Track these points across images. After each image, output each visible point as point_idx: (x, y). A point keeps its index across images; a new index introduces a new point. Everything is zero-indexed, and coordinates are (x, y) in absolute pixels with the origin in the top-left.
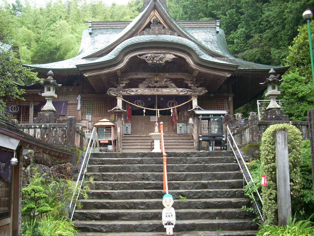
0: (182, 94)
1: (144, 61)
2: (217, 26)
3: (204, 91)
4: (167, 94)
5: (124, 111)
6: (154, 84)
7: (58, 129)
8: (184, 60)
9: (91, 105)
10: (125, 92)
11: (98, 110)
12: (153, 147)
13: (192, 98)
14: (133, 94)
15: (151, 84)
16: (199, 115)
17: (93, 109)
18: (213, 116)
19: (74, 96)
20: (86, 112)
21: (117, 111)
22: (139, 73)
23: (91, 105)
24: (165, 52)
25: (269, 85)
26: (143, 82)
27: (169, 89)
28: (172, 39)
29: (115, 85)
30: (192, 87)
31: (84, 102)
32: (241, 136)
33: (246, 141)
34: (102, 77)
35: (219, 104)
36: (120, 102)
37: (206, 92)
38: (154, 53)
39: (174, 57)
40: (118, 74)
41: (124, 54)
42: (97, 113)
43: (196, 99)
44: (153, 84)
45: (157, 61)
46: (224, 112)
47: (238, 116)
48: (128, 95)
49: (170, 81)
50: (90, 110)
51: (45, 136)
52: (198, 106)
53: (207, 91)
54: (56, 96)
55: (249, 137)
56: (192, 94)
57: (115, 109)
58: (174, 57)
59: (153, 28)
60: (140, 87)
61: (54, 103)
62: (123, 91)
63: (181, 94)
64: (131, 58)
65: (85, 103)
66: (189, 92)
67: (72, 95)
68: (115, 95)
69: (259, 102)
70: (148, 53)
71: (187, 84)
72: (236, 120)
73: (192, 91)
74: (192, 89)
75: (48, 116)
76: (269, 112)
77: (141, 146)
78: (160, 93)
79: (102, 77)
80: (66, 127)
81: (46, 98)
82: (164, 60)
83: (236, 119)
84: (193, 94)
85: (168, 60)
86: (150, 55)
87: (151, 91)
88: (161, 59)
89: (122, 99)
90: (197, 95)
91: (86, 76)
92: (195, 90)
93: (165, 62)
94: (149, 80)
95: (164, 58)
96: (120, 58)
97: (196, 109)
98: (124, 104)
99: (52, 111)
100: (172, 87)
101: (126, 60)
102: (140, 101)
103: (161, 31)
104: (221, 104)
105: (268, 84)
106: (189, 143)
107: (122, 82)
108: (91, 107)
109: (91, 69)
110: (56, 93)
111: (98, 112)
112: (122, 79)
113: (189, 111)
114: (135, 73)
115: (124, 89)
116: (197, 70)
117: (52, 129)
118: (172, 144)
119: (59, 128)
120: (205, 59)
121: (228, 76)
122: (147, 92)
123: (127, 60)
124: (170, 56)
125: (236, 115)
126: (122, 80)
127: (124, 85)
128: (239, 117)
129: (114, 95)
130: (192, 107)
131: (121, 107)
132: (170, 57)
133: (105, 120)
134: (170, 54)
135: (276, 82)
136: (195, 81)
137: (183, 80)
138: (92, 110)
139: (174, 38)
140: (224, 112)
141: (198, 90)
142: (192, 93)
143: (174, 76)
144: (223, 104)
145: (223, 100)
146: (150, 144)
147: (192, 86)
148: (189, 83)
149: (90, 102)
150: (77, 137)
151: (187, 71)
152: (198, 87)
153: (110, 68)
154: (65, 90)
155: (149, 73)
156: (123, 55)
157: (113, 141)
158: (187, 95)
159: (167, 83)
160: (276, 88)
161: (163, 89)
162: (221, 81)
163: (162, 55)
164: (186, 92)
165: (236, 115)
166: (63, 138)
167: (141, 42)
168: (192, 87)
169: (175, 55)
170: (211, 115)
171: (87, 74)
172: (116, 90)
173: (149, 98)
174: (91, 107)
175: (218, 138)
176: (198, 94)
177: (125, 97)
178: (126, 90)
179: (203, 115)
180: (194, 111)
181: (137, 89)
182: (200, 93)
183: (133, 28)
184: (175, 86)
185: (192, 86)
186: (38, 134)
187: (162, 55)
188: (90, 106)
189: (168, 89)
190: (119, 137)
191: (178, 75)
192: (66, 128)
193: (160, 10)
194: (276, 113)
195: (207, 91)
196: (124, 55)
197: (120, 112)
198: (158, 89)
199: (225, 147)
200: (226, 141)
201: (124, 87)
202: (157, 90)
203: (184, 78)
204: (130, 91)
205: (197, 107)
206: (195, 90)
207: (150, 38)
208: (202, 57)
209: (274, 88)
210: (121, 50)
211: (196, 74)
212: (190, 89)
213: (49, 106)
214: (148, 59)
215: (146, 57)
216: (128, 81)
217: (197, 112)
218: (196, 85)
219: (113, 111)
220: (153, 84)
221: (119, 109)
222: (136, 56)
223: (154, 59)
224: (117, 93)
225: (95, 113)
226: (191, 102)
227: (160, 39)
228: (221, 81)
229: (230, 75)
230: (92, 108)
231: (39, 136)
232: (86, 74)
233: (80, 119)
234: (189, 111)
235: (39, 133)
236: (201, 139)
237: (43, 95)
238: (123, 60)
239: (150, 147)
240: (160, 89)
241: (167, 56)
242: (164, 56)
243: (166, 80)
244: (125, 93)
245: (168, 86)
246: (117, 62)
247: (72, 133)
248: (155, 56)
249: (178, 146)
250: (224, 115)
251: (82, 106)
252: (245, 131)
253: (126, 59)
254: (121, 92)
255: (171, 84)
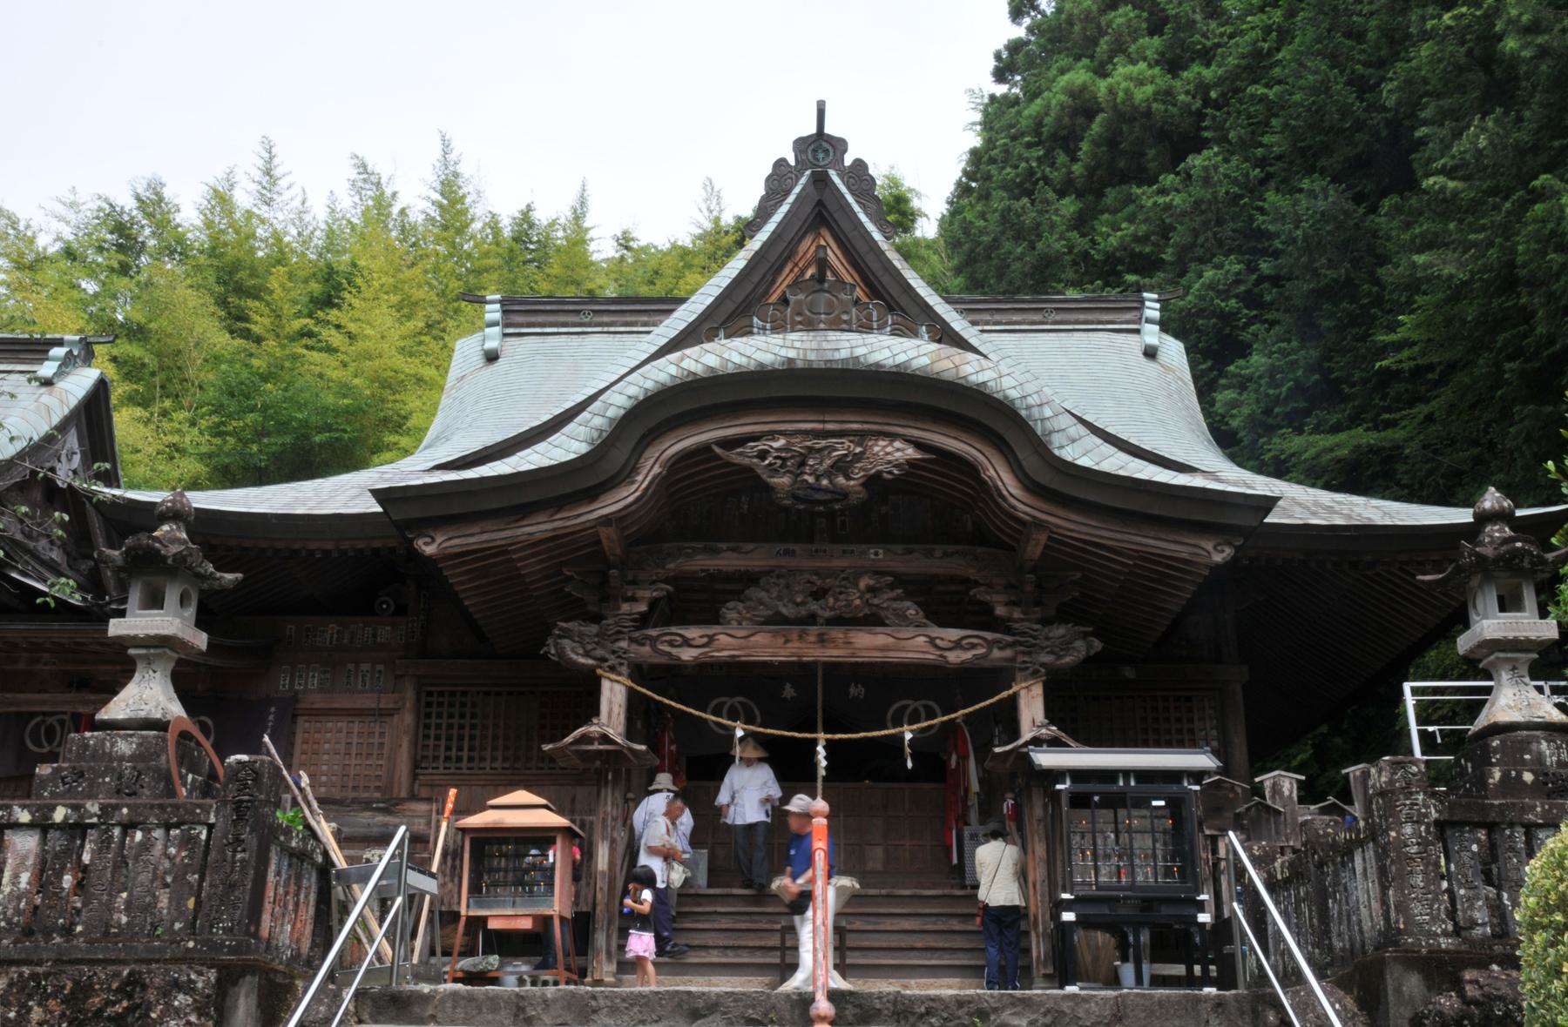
0: (958, 661)
1: (750, 481)
2: (1149, 321)
3: (1079, 644)
4: (877, 656)
5: (630, 749)
6: (803, 603)
7: (158, 833)
8: (969, 469)
9: (467, 721)
10: (643, 645)
11: (506, 748)
12: (788, 960)
13: (1014, 680)
14: (687, 655)
15: (790, 605)
16: (1056, 775)
17: (477, 743)
18: (1137, 781)
19: (380, 667)
20: (436, 758)
21: (596, 746)
22: (724, 546)
23: (467, 721)
24: (866, 427)
25: (1480, 586)
26: (747, 592)
27: (888, 630)
28: (901, 358)
29: (592, 608)
30: (1016, 621)
31: (429, 704)
32: (1321, 898)
33: (1361, 932)
34: (520, 560)
35: (1167, 720)
36: (613, 696)
37: (1092, 652)
38: (805, 433)
39: (911, 452)
40: (605, 542)
41: (638, 436)
42: (497, 764)
43: (1038, 690)
44: (798, 605)
45: (818, 478)
46: (1202, 760)
47: (1276, 789)
48: (663, 660)
49: (892, 587)
50: (460, 749)
51: (68, 881)
52: (1052, 722)
53: (1098, 645)
54: (201, 640)
55: (1375, 905)
56: (1013, 659)
57: (585, 739)
58: (911, 452)
59: (799, 302)
60: (729, 623)
61: (183, 688)
62: (632, 640)
63: (954, 657)
64: (673, 464)
65: (434, 710)
66: (1001, 649)
67: (365, 667)
68: (591, 662)
69: (1415, 691)
70: (772, 435)
71: (987, 609)
72: (1268, 808)
73: (1012, 645)
74: (1014, 635)
75: (132, 758)
76: (1496, 750)
77: (729, 952)
78: (835, 652)
79: (520, 560)
80: (212, 820)
81: (132, 651)
82: (858, 475)
83: (1269, 802)
84: (1020, 658)
85: (879, 474)
86: (781, 442)
87: (787, 642)
88: (842, 466)
89: (629, 683)
90: (1042, 665)
91: (429, 550)
92: (1035, 638)
93: (863, 485)
94: (777, 585)
95: (858, 457)
96: (620, 455)
97: (1036, 742)
98: (635, 705)
99: (160, 725)
100: (904, 620)
101: (650, 469)
102: (741, 699)
103: (845, 317)
104: (1179, 720)
105: (1474, 582)
106: (738, 921)
107: (629, 594)
108: (467, 732)
109: (455, 511)
110: (201, 623)
111: (505, 759)
112: (630, 577)
113: (997, 750)
114: (700, 545)
115: (637, 629)
116: (1039, 525)
117: (117, 832)
118: (907, 941)
119: (168, 827)
120: (1084, 462)
121: (1218, 558)
122: (766, 647)
123: (657, 469)
124: (889, 449)
125: (1267, 779)
126: (634, 582)
127: (643, 608)
128: (1281, 793)
129: (582, 660)
130: (1014, 733)
131: (621, 728)
132: (892, 453)
133: (522, 796)
134: (893, 437)
135: (1526, 564)
136: (1029, 588)
137: (967, 582)
138: (471, 749)
139: (911, 354)
140: (1202, 760)
141: (1047, 638)
142: (1017, 653)
143: (916, 564)
144: (1191, 720)
145: (1189, 699)
146: (774, 941)
147: (1017, 614)
148: (997, 598)
149: (463, 705)
150: (293, 888)
151: (980, 537)
152: (1046, 622)
153: (560, 509)
154: (328, 636)
155: (780, 547)
156: (633, 443)
157: (562, 919)
158: (987, 664)
159: (876, 601)
160: (1530, 599)
161: (852, 634)
162: (1176, 587)
163: (843, 447)
164: (981, 651)
165: (1267, 784)
166: (179, 890)
167: (730, 369)
168: (1016, 621)
169: (918, 445)
170: (1127, 773)
171: (433, 540)
172: (597, 635)
173: (788, 686)
174: (467, 732)
175: (1165, 910)
176: (1046, 658)
177: (640, 673)
178: (653, 632)
179: (1079, 775)
180: (1027, 754)
181: (711, 630)
182: (1060, 657)
183: (705, 320)
184: (921, 613)
185: (1017, 614)
186: (21, 865)
187: (843, 447)
188: (461, 727)
189: (879, 629)
190: (599, 896)
191: (938, 554)
192: (211, 827)
193: (845, 225)
194: (1539, 758)
195: (1098, 645)
196: (638, 443)
197: (608, 752)
198: (824, 629)
199: (1213, 968)
200: (1224, 926)
201: (643, 621)
202: (822, 640)
203: (971, 573)
204: (671, 644)
205: (1044, 731)
206: (1035, 638)
207: (783, 352)
208: (1068, 454)
209: (1508, 603)
210: (622, 412)
211: (1035, 548)
212: (1008, 631)
213: (147, 694)
214: (770, 464)
215: (763, 455)
216: (663, 586)
217: (1046, 759)
218: (1038, 612)
219: (574, 748)
220: (798, 605)
221: (605, 739)
222: (705, 449)
223: (803, 464)
224: (599, 652)
225: (487, 764)
226: (1013, 702)
227: (837, 356)
228: (1176, 587)
229: (1228, 552)
230: (472, 738)
231: (25, 877)
232: (426, 544)
233: (404, 794)
234: (997, 750)
235: (24, 858)
236: (1068, 916)
237: (116, 628)
238: (634, 470)
239: (777, 961)
240: (837, 633)
241: (876, 449)
242: (858, 450)
243: (872, 582)
244: (647, 649)
245: (882, 614)
246: (602, 478)
247: (242, 860)
248: (810, 449)
249: (939, 958)
250: (1197, 775)
251: (417, 726)
252: (1344, 864)
253: (653, 460)
254: (624, 644)
255: (896, 605)
